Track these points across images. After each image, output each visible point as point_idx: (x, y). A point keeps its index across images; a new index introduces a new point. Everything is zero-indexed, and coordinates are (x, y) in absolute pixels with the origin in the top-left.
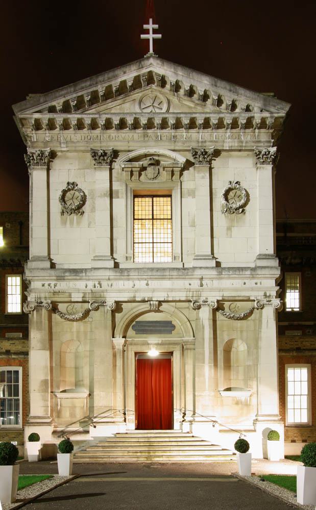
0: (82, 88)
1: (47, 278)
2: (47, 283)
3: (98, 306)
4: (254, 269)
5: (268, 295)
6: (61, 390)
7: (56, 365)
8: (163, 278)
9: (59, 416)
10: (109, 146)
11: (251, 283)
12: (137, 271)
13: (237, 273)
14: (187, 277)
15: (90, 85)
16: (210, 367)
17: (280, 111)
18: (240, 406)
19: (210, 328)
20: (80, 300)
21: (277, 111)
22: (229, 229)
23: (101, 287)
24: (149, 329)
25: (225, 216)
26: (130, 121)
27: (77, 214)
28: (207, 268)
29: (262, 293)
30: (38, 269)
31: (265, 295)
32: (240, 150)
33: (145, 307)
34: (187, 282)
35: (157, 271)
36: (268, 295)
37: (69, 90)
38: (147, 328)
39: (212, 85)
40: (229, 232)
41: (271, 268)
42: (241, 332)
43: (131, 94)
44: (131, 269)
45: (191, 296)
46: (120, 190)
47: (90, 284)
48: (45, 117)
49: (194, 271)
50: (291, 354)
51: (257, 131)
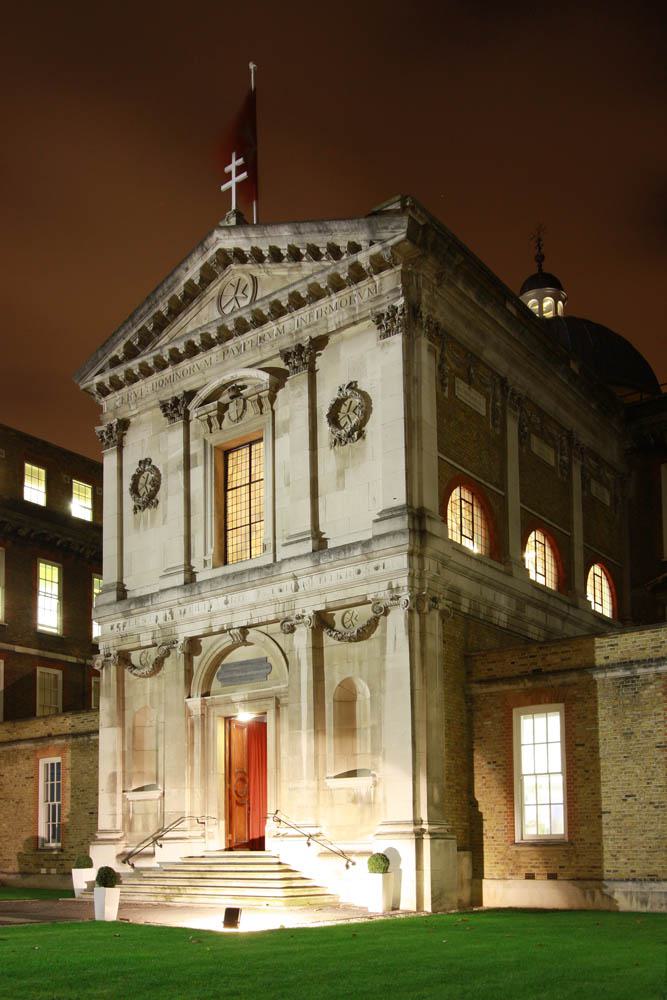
0: (141, 317)
1: (113, 617)
2: (115, 624)
3: (168, 649)
4: (366, 544)
5: (394, 587)
6: (134, 787)
7: (129, 748)
8: (243, 588)
9: (131, 830)
10: (177, 389)
11: (367, 569)
13: (342, 556)
14: (273, 579)
15: (150, 308)
16: (309, 734)
17: (396, 233)
18: (359, 805)
19: (308, 664)
20: (150, 643)
21: (393, 234)
22: (341, 474)
25: (335, 453)
26: (197, 340)
27: (150, 508)
28: (299, 557)
29: (385, 585)
31: (390, 588)
32: (355, 323)
34: (276, 587)
35: (234, 578)
36: (394, 587)
37: (127, 328)
39: (295, 233)
41: (393, 534)
42: (360, 663)
43: (207, 291)
45: (281, 610)
47: (161, 614)
48: (105, 378)
49: (280, 567)
50: (522, 686)
51: (376, 278)
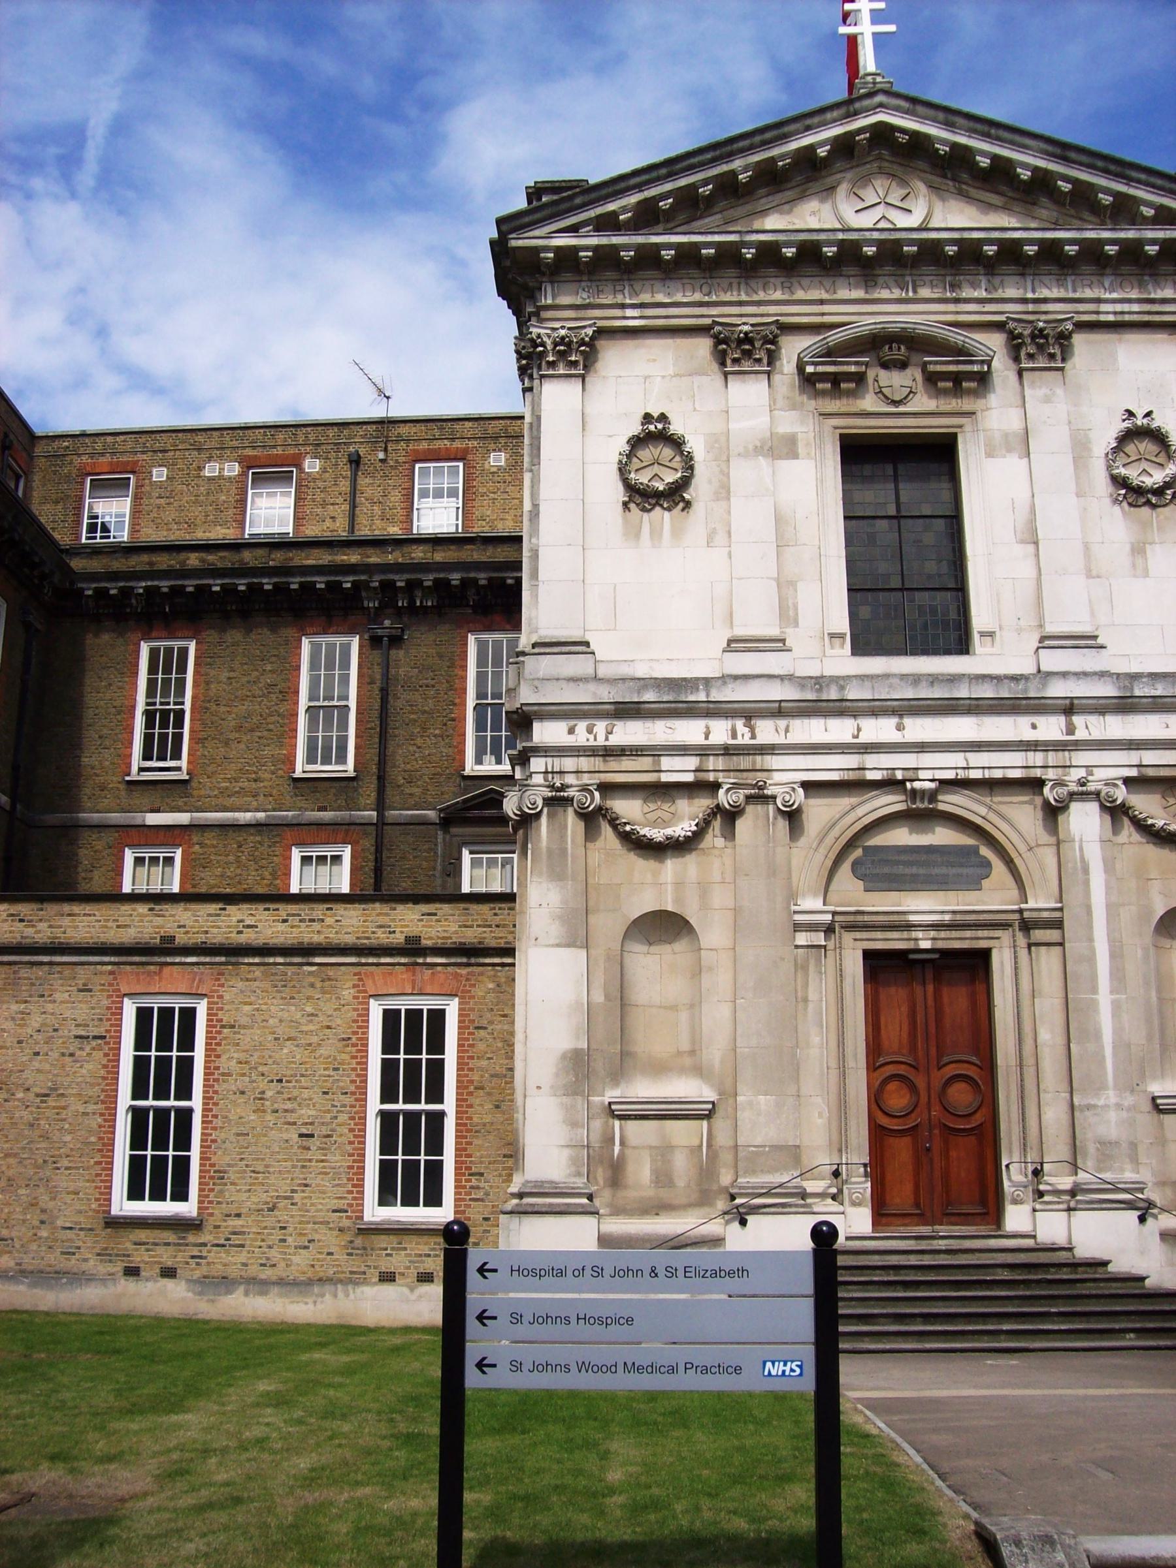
12: (867, 684)
23: (753, 737)
24: (907, 871)
30: (558, 679)
33: (890, 803)
38: (901, 870)
40: (1139, 561)
44: (848, 678)
46: (800, 436)
